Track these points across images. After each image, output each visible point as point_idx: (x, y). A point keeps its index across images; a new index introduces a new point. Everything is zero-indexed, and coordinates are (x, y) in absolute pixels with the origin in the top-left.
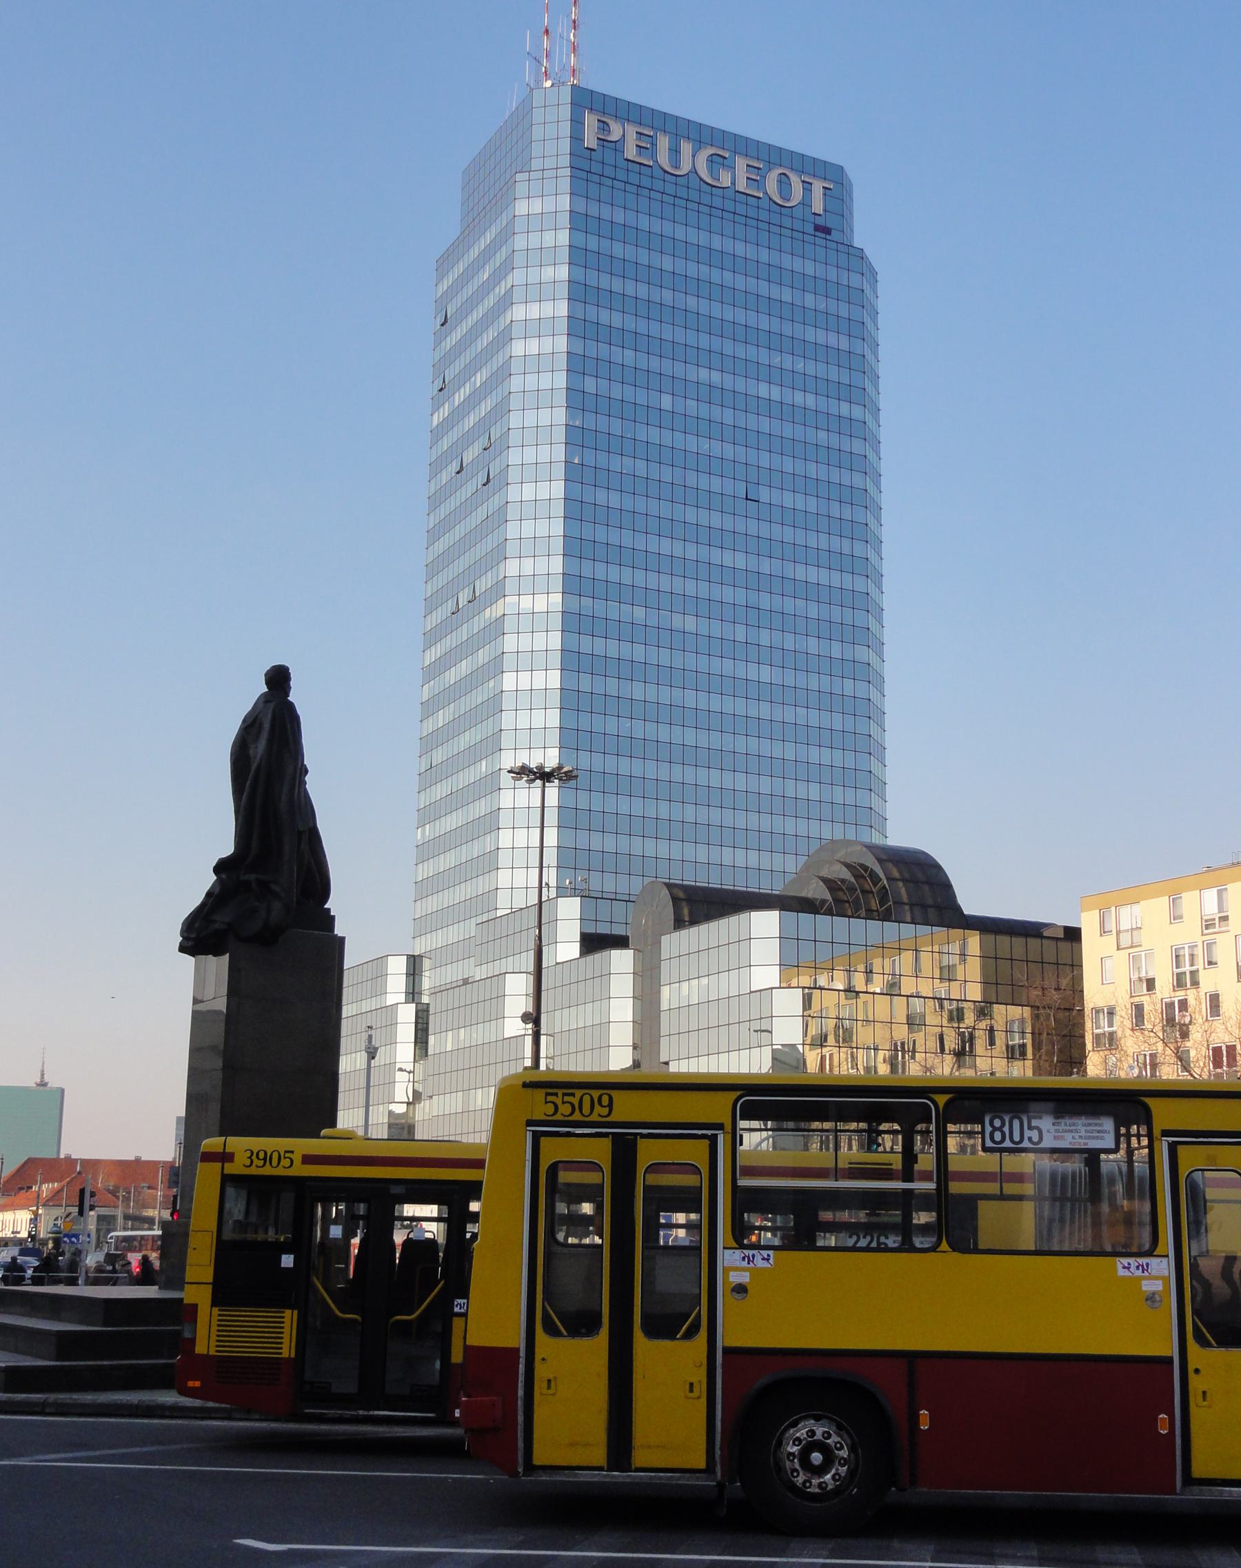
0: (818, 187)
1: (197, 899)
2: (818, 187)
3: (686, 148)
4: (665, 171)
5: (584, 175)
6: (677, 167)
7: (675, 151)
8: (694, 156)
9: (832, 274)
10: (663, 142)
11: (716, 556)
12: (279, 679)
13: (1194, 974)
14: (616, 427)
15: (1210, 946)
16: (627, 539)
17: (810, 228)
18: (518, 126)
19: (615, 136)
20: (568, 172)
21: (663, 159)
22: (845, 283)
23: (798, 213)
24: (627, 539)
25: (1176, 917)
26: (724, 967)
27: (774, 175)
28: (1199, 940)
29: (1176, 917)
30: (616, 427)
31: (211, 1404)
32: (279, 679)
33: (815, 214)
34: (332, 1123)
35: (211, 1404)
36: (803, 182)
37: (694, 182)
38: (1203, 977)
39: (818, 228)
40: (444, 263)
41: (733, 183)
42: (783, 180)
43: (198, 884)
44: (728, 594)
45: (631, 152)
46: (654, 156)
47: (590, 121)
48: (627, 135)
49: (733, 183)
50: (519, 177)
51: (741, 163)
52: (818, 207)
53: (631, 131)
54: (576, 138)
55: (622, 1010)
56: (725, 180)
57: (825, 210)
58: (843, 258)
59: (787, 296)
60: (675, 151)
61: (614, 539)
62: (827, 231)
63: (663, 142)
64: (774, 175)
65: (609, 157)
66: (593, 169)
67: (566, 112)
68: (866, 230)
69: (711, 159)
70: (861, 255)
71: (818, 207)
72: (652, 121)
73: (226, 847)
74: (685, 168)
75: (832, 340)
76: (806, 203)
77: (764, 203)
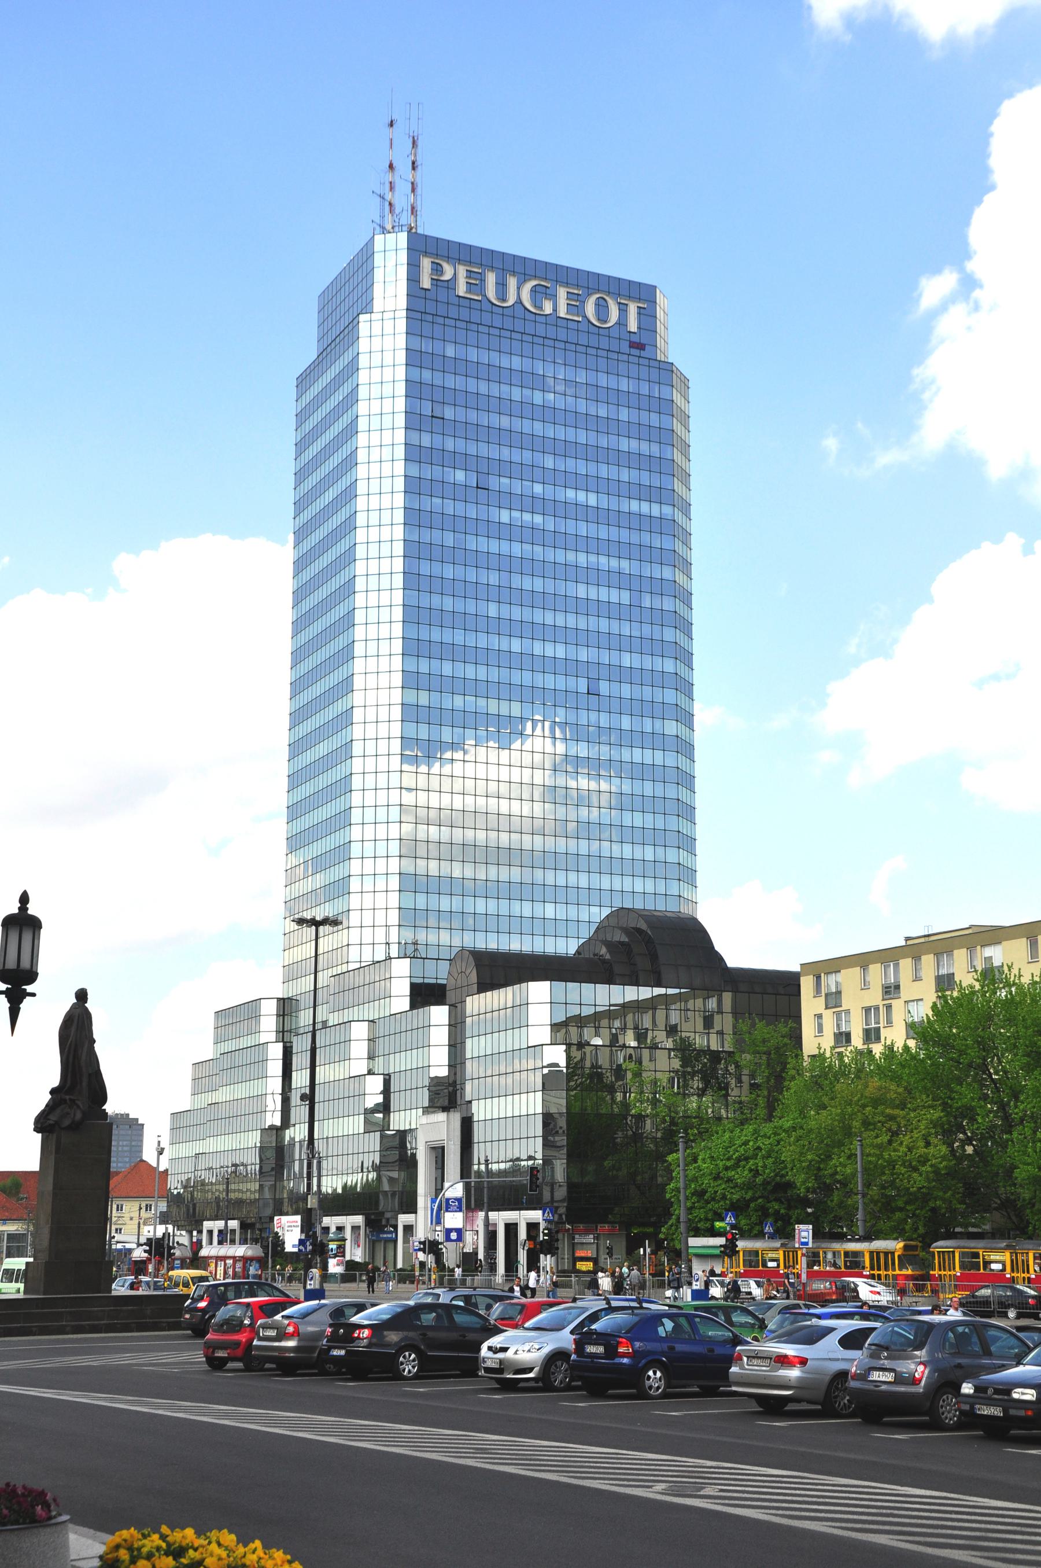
0: (633, 308)
1: (42, 1106)
2: (633, 308)
3: (512, 282)
4: (493, 304)
5: (418, 316)
6: (504, 300)
7: (502, 285)
8: (518, 288)
9: (645, 389)
10: (491, 278)
11: (538, 648)
12: (82, 996)
13: (878, 1030)
14: (449, 539)
15: (889, 1007)
16: (459, 637)
17: (625, 347)
18: (360, 271)
19: (448, 275)
20: (404, 313)
21: (491, 293)
22: (657, 395)
23: (614, 333)
24: (459, 637)
25: (865, 986)
26: (489, 1030)
27: (592, 299)
28: (881, 1003)
29: (865, 986)
30: (449, 539)
31: (671, 991)
32: (82, 996)
33: (630, 332)
34: (896, 403)
35: (671, 991)
36: (620, 303)
37: (519, 309)
38: (883, 1033)
39: (633, 345)
40: (304, 381)
41: (555, 310)
42: (601, 307)
43: (42, 1100)
44: (550, 681)
45: (462, 289)
46: (483, 293)
47: (426, 263)
48: (457, 274)
49: (555, 310)
50: (362, 317)
51: (562, 293)
52: (633, 326)
53: (462, 271)
54: (413, 279)
55: (440, 1035)
56: (548, 308)
57: (639, 328)
58: (654, 373)
59: (602, 412)
60: (502, 285)
61: (447, 638)
62: (641, 347)
63: (491, 278)
64: (592, 299)
65: (442, 296)
66: (426, 309)
67: (403, 257)
68: (676, 345)
69: (534, 290)
70: (668, 368)
71: (633, 326)
72: (479, 259)
73: (56, 1082)
74: (511, 300)
75: (645, 448)
76: (622, 323)
77: (583, 327)
